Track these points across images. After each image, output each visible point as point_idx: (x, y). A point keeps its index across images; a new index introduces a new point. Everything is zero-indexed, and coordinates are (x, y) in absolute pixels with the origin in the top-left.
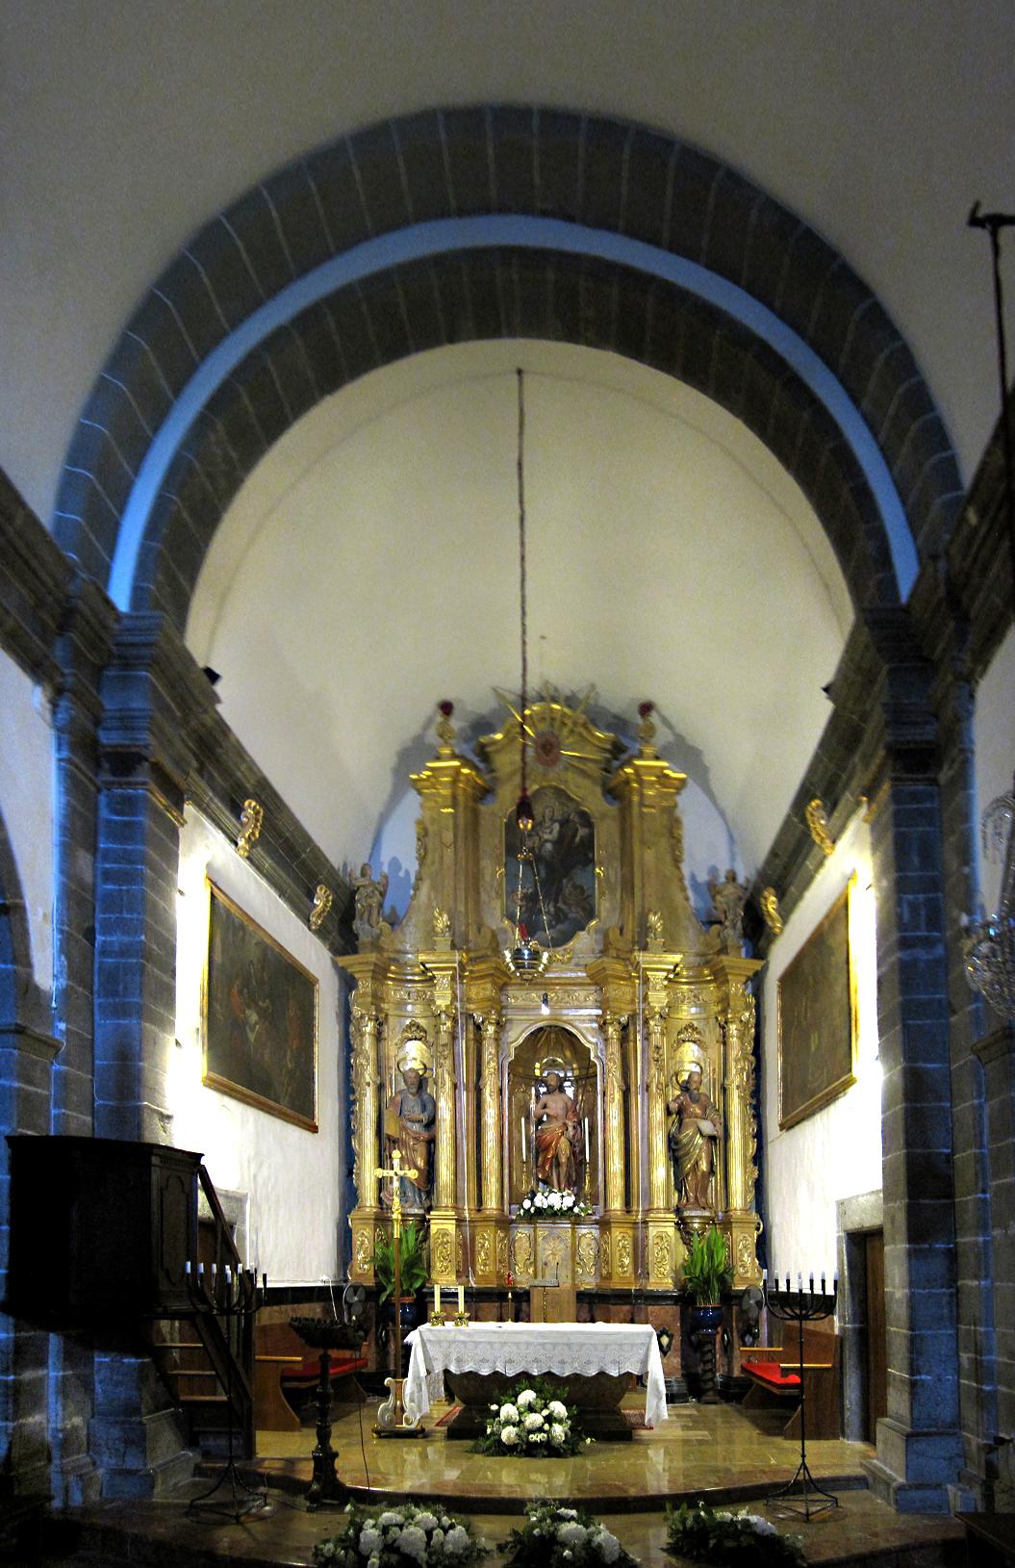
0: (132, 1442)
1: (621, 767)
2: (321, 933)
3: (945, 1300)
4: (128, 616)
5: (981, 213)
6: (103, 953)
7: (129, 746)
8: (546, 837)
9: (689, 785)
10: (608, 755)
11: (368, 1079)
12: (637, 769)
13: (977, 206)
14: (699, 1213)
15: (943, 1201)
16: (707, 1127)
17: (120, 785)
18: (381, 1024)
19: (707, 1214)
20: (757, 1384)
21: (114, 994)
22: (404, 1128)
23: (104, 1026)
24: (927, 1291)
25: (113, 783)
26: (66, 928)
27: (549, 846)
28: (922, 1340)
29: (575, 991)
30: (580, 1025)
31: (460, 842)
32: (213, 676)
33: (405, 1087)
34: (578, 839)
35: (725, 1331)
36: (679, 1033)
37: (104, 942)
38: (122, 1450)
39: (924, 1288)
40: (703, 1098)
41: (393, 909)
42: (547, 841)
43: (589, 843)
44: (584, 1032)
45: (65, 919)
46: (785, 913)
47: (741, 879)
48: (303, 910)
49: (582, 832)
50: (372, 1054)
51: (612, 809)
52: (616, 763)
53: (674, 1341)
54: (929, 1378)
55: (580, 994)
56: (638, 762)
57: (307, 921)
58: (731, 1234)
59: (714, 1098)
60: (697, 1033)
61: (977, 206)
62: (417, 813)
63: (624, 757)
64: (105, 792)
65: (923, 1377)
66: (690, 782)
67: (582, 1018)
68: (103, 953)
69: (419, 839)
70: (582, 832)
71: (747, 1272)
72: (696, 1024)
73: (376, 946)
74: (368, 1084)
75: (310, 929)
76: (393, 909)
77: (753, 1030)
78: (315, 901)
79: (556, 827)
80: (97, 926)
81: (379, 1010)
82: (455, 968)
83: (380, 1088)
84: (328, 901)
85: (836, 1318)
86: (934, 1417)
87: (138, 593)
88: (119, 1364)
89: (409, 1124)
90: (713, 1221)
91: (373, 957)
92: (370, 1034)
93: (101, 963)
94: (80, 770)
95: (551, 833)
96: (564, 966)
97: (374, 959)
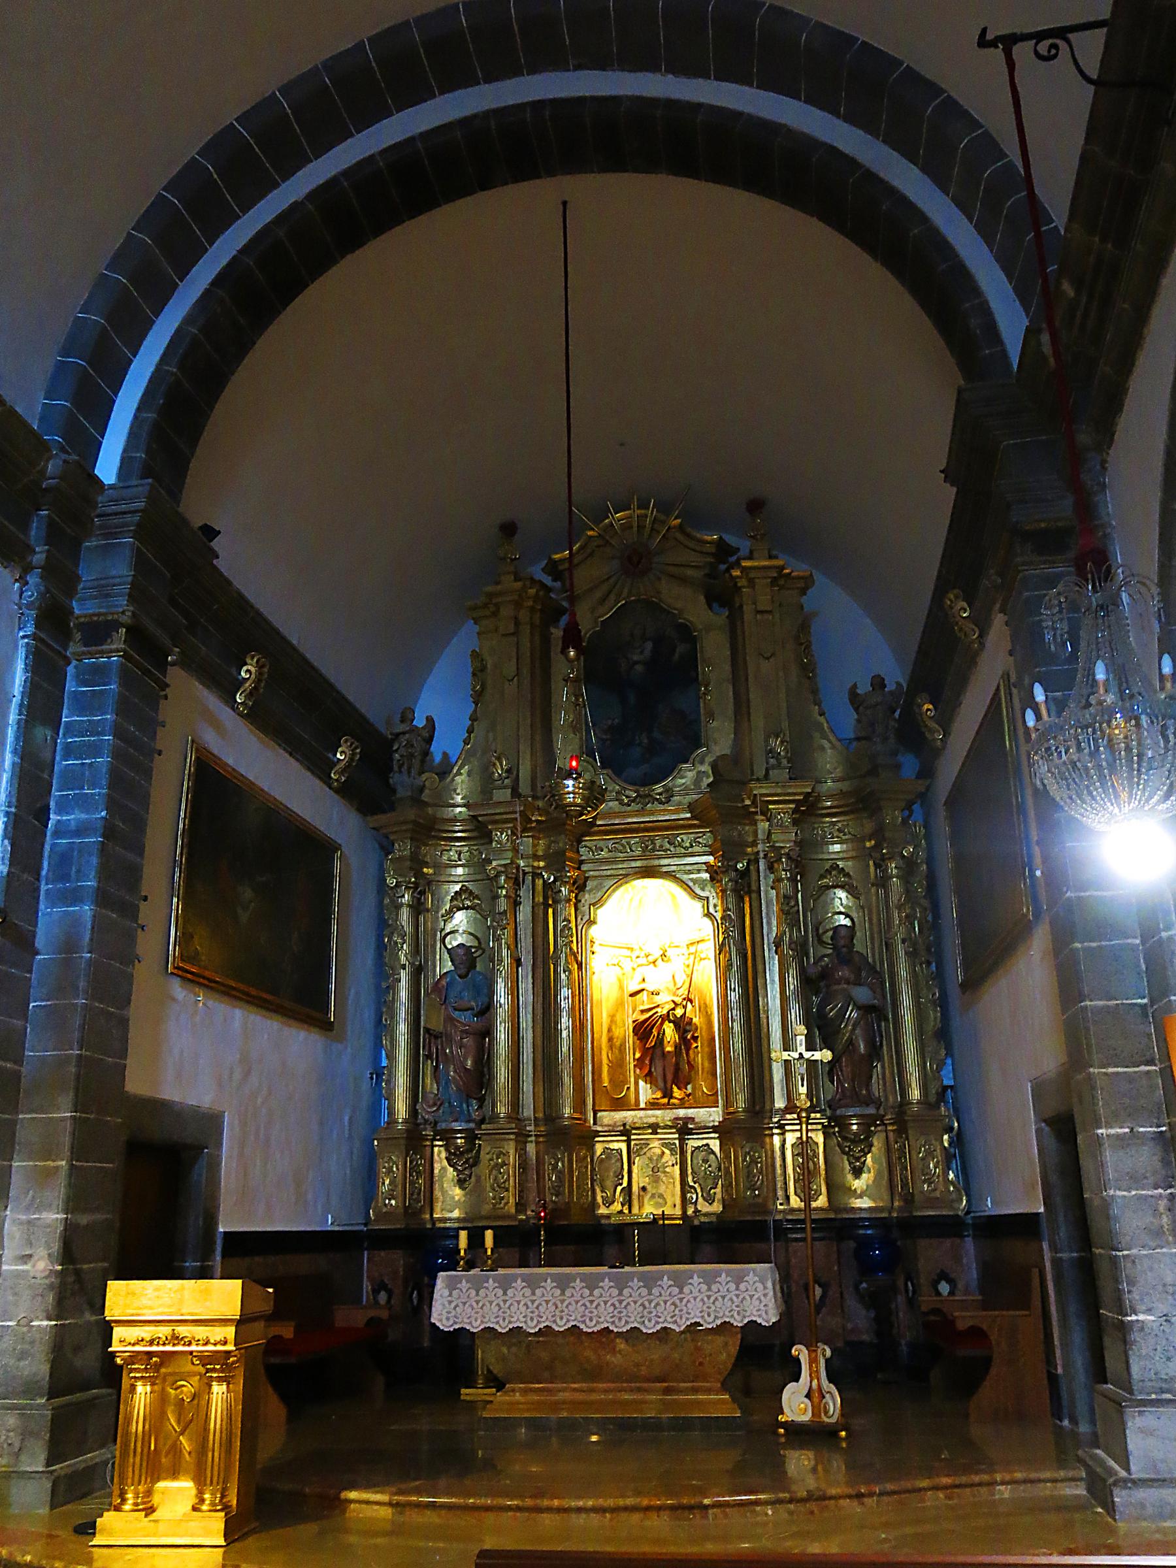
0: (31, 1433)
1: (728, 570)
2: (345, 791)
3: (1162, 1205)
4: (111, 487)
5: (990, 36)
6: (57, 834)
7: (105, 614)
8: (635, 658)
9: (817, 583)
10: (710, 559)
11: (403, 960)
12: (744, 569)
13: (984, 31)
14: (858, 1110)
15: (1143, 1068)
16: (862, 994)
17: (91, 655)
18: (423, 893)
19: (871, 1111)
20: (634, 1265)
21: (65, 877)
22: (450, 1020)
23: (50, 914)
24: (1134, 1193)
25: (84, 653)
26: (13, 810)
27: (639, 668)
28: (1134, 1262)
29: (678, 835)
30: (685, 877)
31: (525, 671)
32: (210, 532)
33: (453, 968)
34: (677, 656)
35: (909, 1278)
36: (822, 877)
37: (59, 821)
38: (17, 1445)
39: (1129, 1190)
40: (857, 958)
41: (445, 754)
42: (636, 663)
43: (691, 661)
44: (691, 884)
45: (14, 800)
46: (945, 721)
47: (890, 687)
48: (320, 767)
49: (681, 648)
50: (408, 928)
51: (720, 618)
52: (723, 567)
53: (830, 1293)
54: (1152, 1318)
55: (686, 838)
56: (744, 564)
57: (327, 780)
58: (907, 1138)
59: (873, 955)
60: (844, 876)
61: (984, 31)
62: (474, 644)
63: (733, 559)
64: (74, 663)
65: (1141, 1317)
66: (818, 576)
67: (688, 868)
68: (57, 834)
69: (474, 674)
70: (681, 648)
71: (935, 1190)
72: (841, 864)
73: (416, 800)
74: (403, 966)
75: (330, 788)
76: (445, 754)
77: (925, 867)
78: (338, 756)
79: (649, 646)
80: (52, 804)
81: (419, 874)
82: (516, 819)
83: (418, 972)
84: (354, 754)
85: (1045, 1246)
86: (1164, 1377)
87: (124, 470)
88: (25, 1329)
89: (456, 1014)
90: (882, 1121)
91: (411, 814)
92: (409, 906)
93: (53, 845)
94: (48, 646)
95: (642, 653)
96: (662, 807)
97: (413, 817)
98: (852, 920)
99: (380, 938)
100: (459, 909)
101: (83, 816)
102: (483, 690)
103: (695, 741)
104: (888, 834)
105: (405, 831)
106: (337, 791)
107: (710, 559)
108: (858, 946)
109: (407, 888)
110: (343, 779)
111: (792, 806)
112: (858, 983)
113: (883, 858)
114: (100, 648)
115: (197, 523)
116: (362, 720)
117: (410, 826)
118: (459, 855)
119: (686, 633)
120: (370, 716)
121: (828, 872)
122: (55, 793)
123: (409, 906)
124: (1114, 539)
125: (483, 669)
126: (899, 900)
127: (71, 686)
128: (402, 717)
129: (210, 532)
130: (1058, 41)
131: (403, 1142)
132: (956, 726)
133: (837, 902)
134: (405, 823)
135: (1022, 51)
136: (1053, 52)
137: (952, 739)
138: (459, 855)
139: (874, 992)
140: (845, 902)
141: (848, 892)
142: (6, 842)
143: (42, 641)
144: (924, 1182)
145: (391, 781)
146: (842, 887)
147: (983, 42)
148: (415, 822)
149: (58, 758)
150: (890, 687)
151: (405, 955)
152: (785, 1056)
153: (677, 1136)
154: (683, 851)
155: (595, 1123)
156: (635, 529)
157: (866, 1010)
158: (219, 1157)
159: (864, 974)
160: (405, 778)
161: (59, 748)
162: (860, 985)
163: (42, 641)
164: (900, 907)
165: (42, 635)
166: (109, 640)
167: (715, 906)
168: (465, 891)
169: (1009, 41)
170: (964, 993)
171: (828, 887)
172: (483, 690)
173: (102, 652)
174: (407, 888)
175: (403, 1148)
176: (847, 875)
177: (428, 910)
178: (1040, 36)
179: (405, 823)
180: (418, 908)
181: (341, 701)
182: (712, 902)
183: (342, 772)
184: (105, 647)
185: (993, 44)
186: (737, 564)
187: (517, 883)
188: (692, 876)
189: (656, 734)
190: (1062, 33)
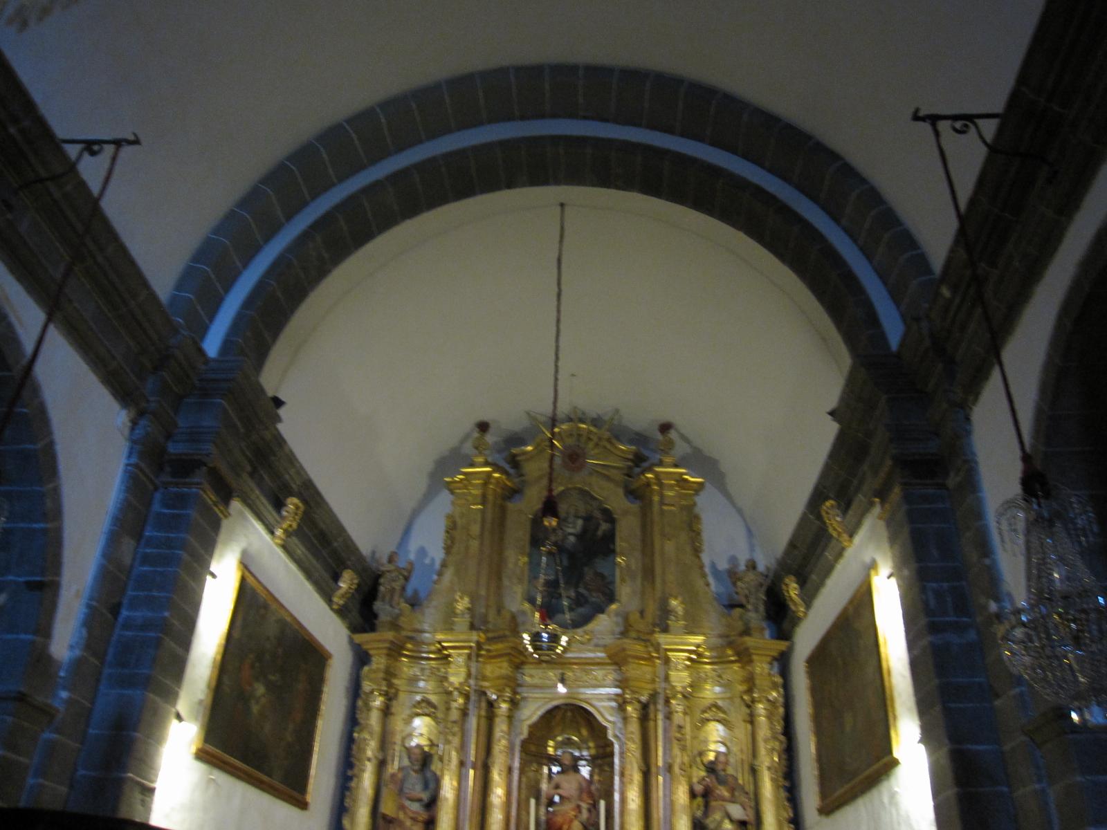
2: (342, 612)
4: (214, 360)
5: (921, 114)
8: (571, 530)
10: (630, 463)
16: (736, 811)
17: (177, 485)
22: (402, 808)
27: (572, 539)
32: (278, 403)
43: (610, 537)
44: (602, 710)
46: (808, 600)
47: (761, 567)
49: (604, 527)
51: (635, 507)
52: (637, 470)
55: (598, 673)
57: (329, 601)
62: (448, 509)
63: (645, 465)
66: (708, 485)
70: (604, 527)
73: (395, 626)
79: (580, 522)
80: (125, 601)
81: (390, 685)
83: (382, 764)
89: (407, 803)
91: (390, 635)
92: (378, 709)
101: (149, 614)
103: (611, 598)
104: (757, 682)
105: (382, 648)
107: (630, 463)
111: (466, 651)
112: (733, 800)
113: (753, 701)
114: (183, 480)
115: (270, 393)
116: (360, 558)
117: (387, 645)
119: (609, 516)
122: (130, 593)
123: (378, 709)
124: (632, 503)
127: (156, 507)
129: (278, 403)
130: (968, 123)
133: (715, 733)
134: (384, 641)
135: (944, 126)
136: (965, 129)
147: (916, 117)
148: (392, 642)
150: (761, 567)
162: (733, 802)
164: (766, 741)
165: (143, 465)
169: (934, 119)
178: (955, 118)
183: (343, 596)
184: (187, 480)
185: (923, 119)
186: (650, 469)
189: (582, 590)
190: (970, 118)
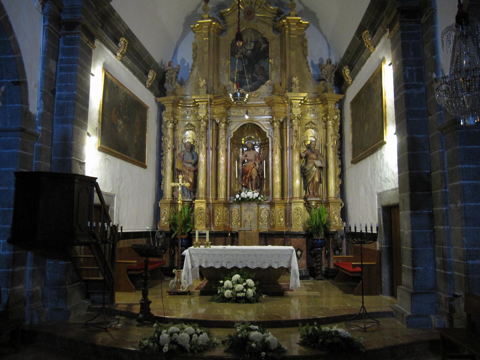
2: (151, 89)
6: (59, 99)
8: (248, 48)
12: (288, 21)
14: (314, 199)
16: (318, 163)
17: (68, 34)
19: (318, 199)
22: (184, 166)
26: (44, 90)
27: (249, 52)
34: (262, 49)
35: (326, 249)
36: (306, 125)
40: (316, 151)
42: (248, 50)
43: (267, 50)
44: (264, 125)
45: (43, 86)
47: (333, 62)
51: (277, 36)
52: (278, 19)
53: (303, 253)
55: (262, 110)
56: (288, 18)
57: (145, 84)
60: (314, 125)
63: (283, 16)
68: (59, 99)
70: (264, 46)
73: (174, 93)
79: (253, 44)
80: (57, 88)
82: (208, 101)
83: (174, 150)
89: (186, 164)
92: (170, 128)
95: (250, 46)
98: (316, 139)
99: (160, 138)
100: (188, 130)
102: (196, 56)
106: (148, 88)
108: (316, 148)
109: (170, 122)
110: (150, 84)
114: (71, 32)
117: (172, 102)
118: (188, 112)
119: (266, 41)
120: (157, 62)
121: (309, 123)
123: (170, 128)
125: (197, 49)
126: (332, 133)
127: (62, 45)
128: (169, 64)
131: (169, 204)
132: (357, 77)
134: (170, 100)
137: (354, 82)
138: (188, 112)
139: (322, 163)
140: (313, 133)
141: (315, 130)
142: (42, 101)
143: (50, 27)
144: (333, 221)
145: (165, 86)
146: (313, 128)
149: (58, 72)
151: (170, 145)
152: (173, 184)
153: (257, 205)
154: (262, 114)
155: (230, 200)
156: (250, 3)
157: (321, 168)
158: (114, 209)
159: (319, 157)
160: (170, 86)
161: (58, 68)
163: (50, 27)
165: (51, 25)
166: (75, 29)
167: (271, 133)
168: (189, 124)
170: (352, 164)
171: (308, 128)
172: (196, 56)
173: (72, 33)
174: (170, 122)
175: (169, 206)
176: (194, 127)
177: (177, 130)
179: (170, 100)
180: (174, 129)
181: (150, 58)
182: (271, 131)
187: (207, 122)
188: (264, 123)
189: (254, 75)
